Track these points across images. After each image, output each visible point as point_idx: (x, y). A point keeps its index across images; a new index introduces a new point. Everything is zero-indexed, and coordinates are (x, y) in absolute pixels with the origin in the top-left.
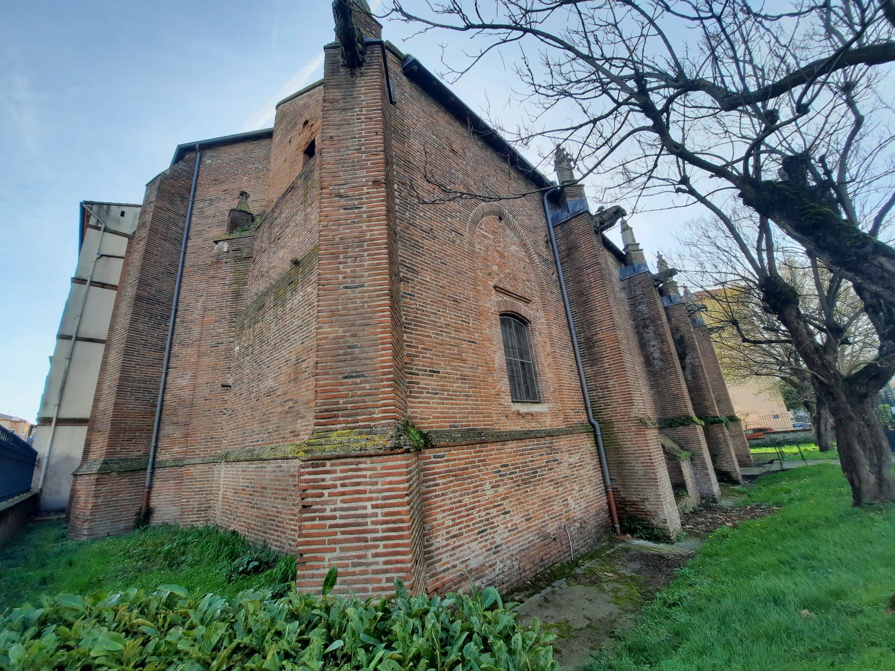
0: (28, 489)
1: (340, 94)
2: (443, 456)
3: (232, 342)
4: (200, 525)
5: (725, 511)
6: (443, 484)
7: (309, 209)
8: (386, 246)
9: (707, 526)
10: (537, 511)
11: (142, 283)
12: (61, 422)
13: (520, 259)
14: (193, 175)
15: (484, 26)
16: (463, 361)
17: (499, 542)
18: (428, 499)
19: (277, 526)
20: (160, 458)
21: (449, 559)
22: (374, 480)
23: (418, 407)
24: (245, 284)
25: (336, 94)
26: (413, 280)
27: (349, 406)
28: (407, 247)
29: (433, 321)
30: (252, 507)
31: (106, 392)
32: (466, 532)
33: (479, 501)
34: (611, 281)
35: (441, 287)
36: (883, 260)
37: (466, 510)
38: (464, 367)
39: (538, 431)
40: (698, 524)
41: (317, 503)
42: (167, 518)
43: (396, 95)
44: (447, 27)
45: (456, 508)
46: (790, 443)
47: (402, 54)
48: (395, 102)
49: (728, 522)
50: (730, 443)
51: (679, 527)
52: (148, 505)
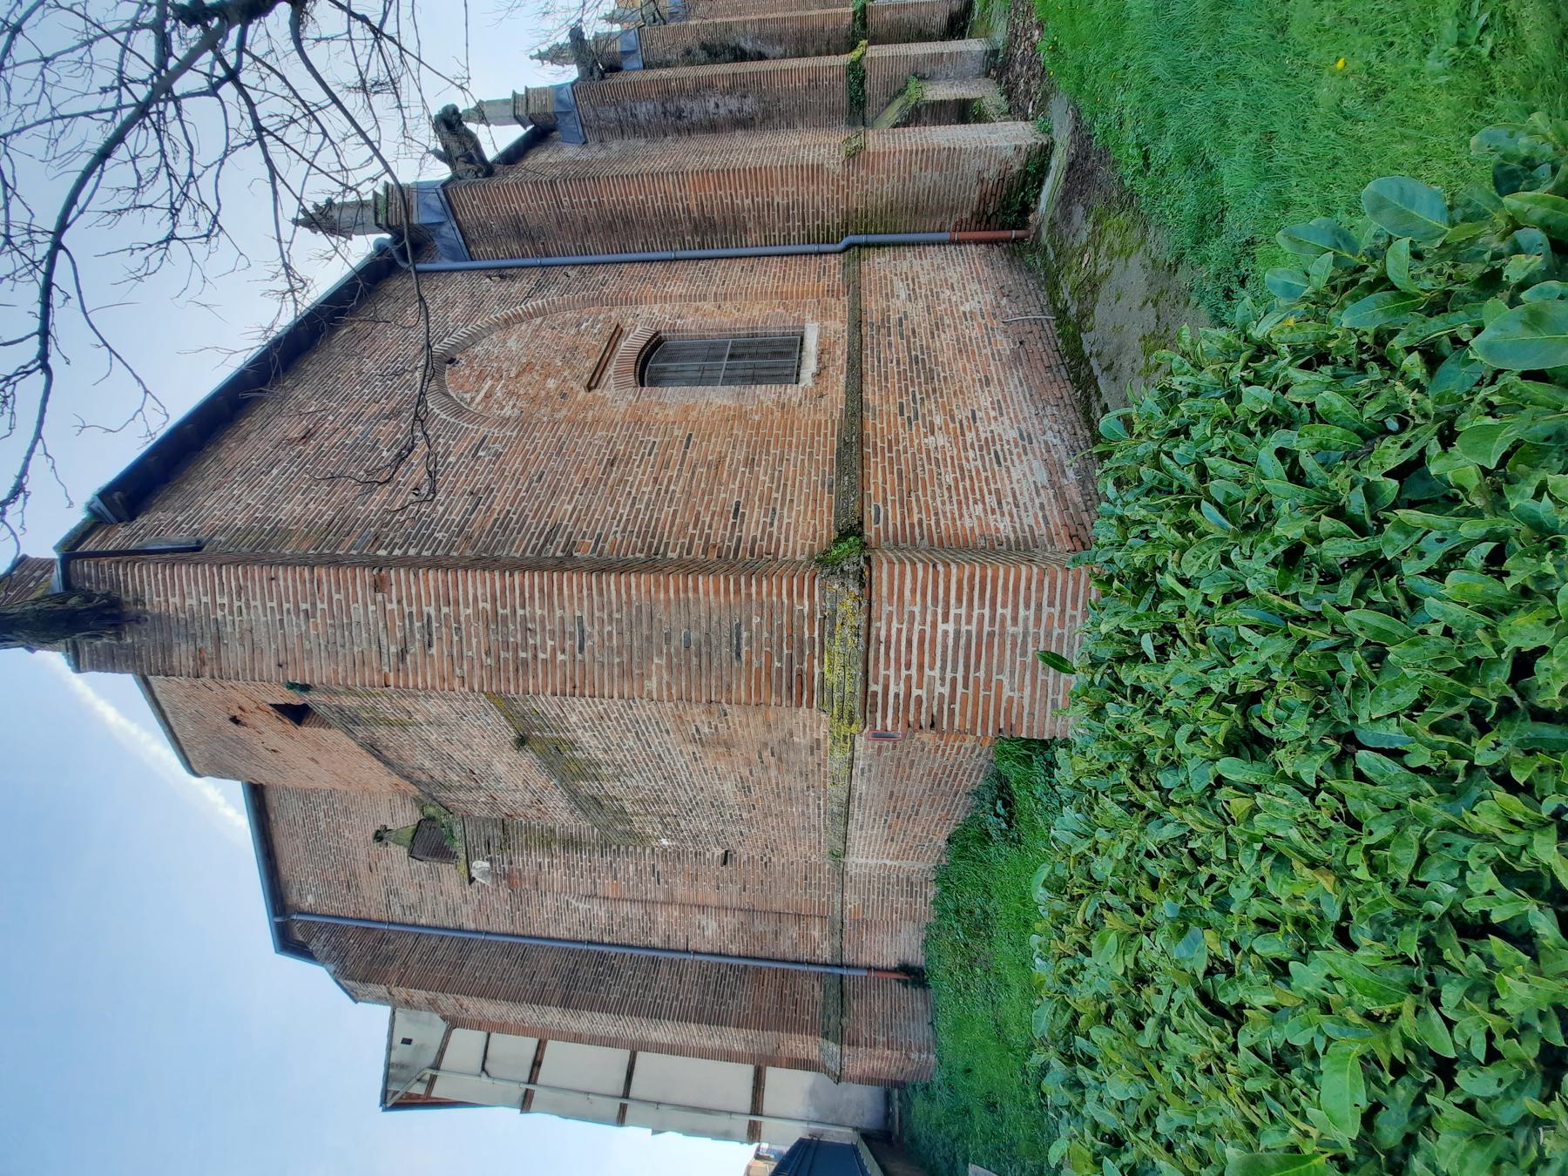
0: (854, 1149)
1: (184, 647)
2: (877, 509)
3: (653, 850)
4: (932, 891)
7: (419, 717)
8: (507, 574)
9: (1034, 76)
10: (976, 365)
11: (539, 998)
12: (756, 1108)
14: (337, 925)
15: (45, 333)
17: (1014, 434)
18: (940, 539)
19: (949, 776)
20: (827, 957)
21: (1030, 513)
22: (906, 617)
23: (795, 542)
24: (552, 831)
25: (183, 654)
26: (571, 533)
27: (785, 651)
28: (507, 540)
30: (917, 814)
31: (718, 1042)
32: (996, 483)
33: (952, 458)
34: (589, 164)
35: (585, 486)
37: (963, 479)
38: (732, 460)
39: (851, 344)
40: (1028, 91)
41: (930, 707)
42: (916, 942)
43: (182, 538)
44: (43, 410)
45: (958, 495)
47: (85, 521)
49: (1032, 36)
51: (1029, 126)
52: (895, 971)
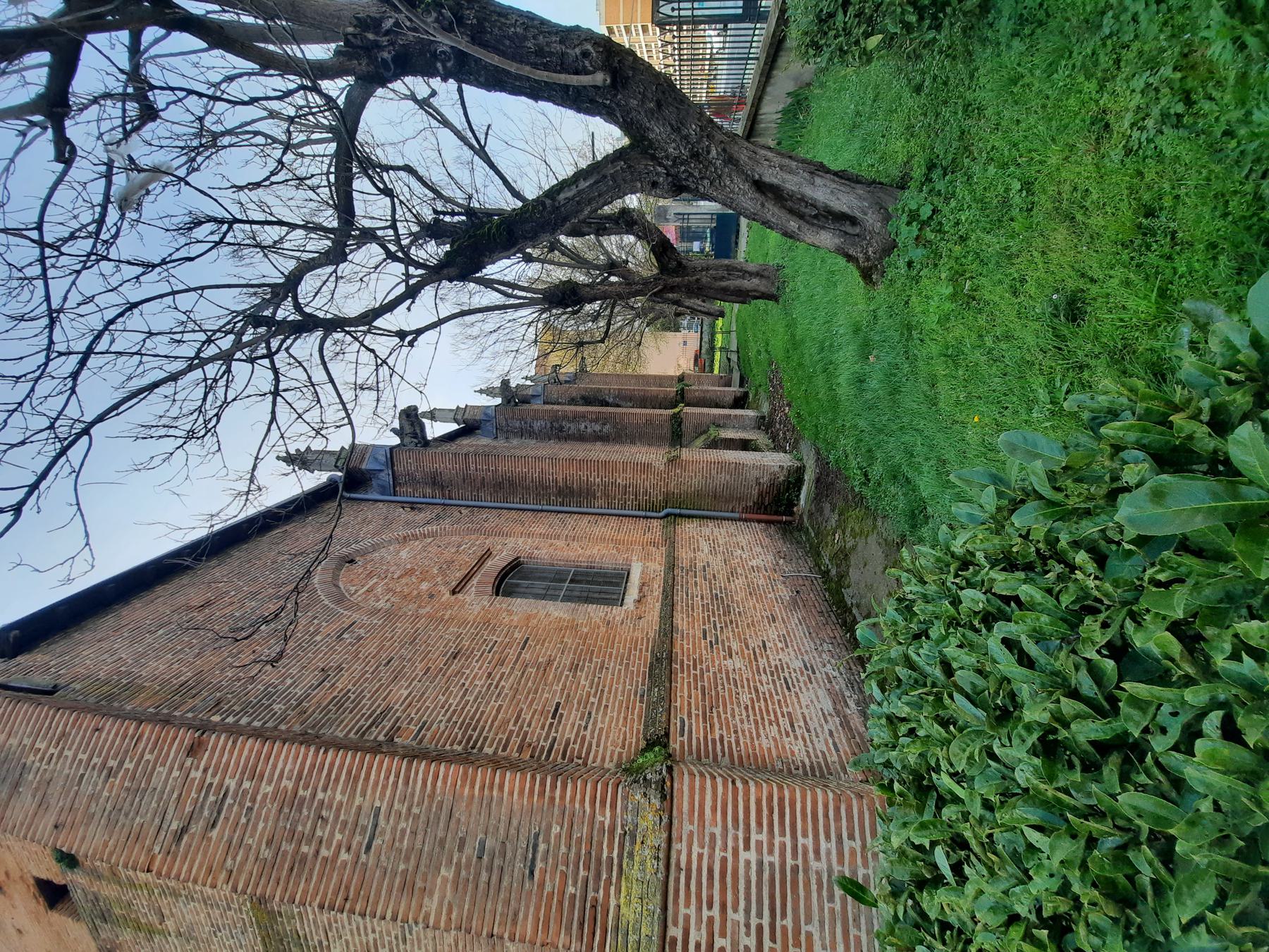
2: (683, 721)
5: (773, 411)
6: (721, 729)
8: (322, 751)
13: (424, 549)
16: (550, 662)
18: (740, 757)
21: (821, 739)
22: (707, 839)
23: (605, 748)
26: (398, 719)
29: (477, 698)
32: (787, 706)
33: (748, 680)
36: (562, 196)
37: (759, 701)
39: (666, 581)
43: (43, 681)
45: (755, 715)
46: (712, 340)
48: (55, 686)
50: (705, 388)
